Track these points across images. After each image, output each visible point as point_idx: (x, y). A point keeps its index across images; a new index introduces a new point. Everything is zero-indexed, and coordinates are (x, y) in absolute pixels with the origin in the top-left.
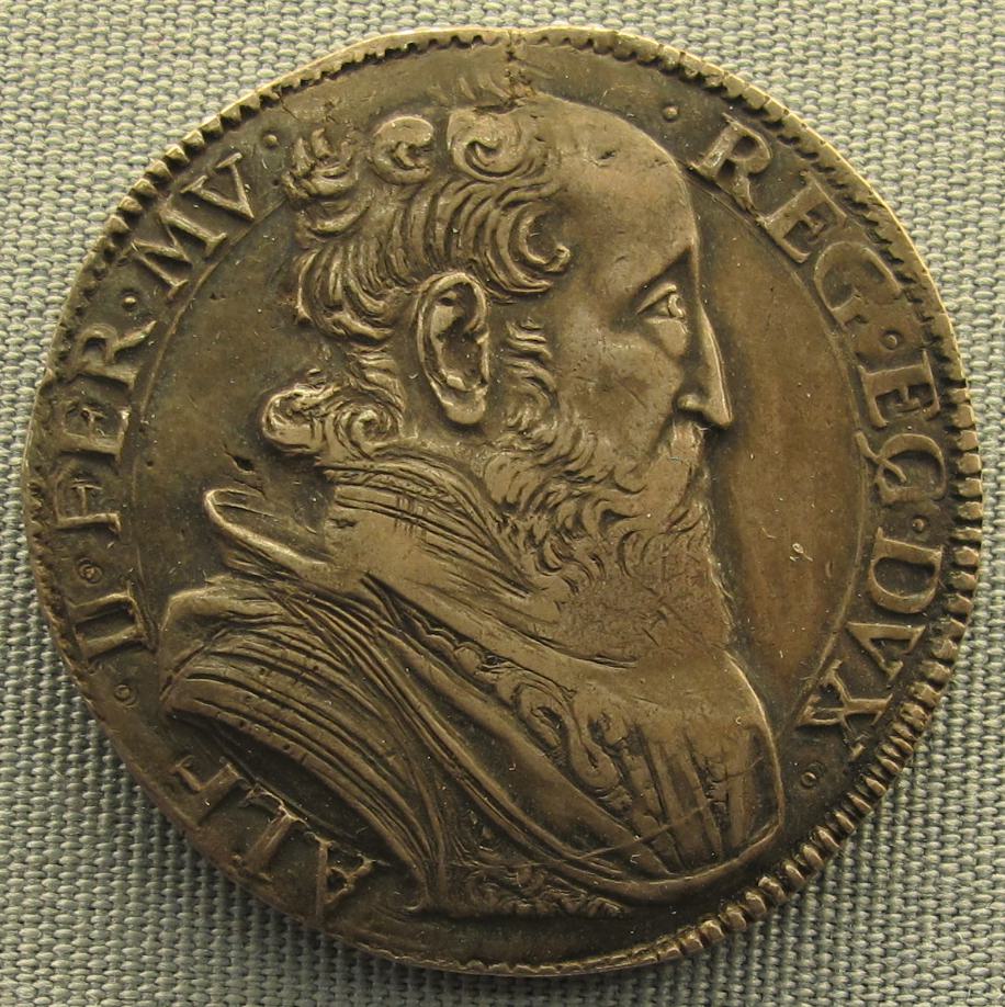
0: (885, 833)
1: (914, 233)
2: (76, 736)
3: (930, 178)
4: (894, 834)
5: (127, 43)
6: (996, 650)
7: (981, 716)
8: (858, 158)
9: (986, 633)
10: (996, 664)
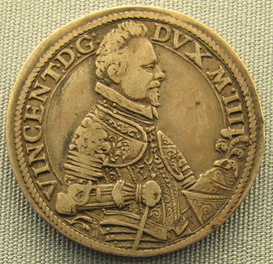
0: (232, 226)
1: (241, 56)
2: (18, 194)
3: (255, 261)
4: (234, 226)
5: (10, 34)
6: (271, 161)
7: (266, 214)
8: (220, 33)
9: (266, 200)
10: (271, 173)
